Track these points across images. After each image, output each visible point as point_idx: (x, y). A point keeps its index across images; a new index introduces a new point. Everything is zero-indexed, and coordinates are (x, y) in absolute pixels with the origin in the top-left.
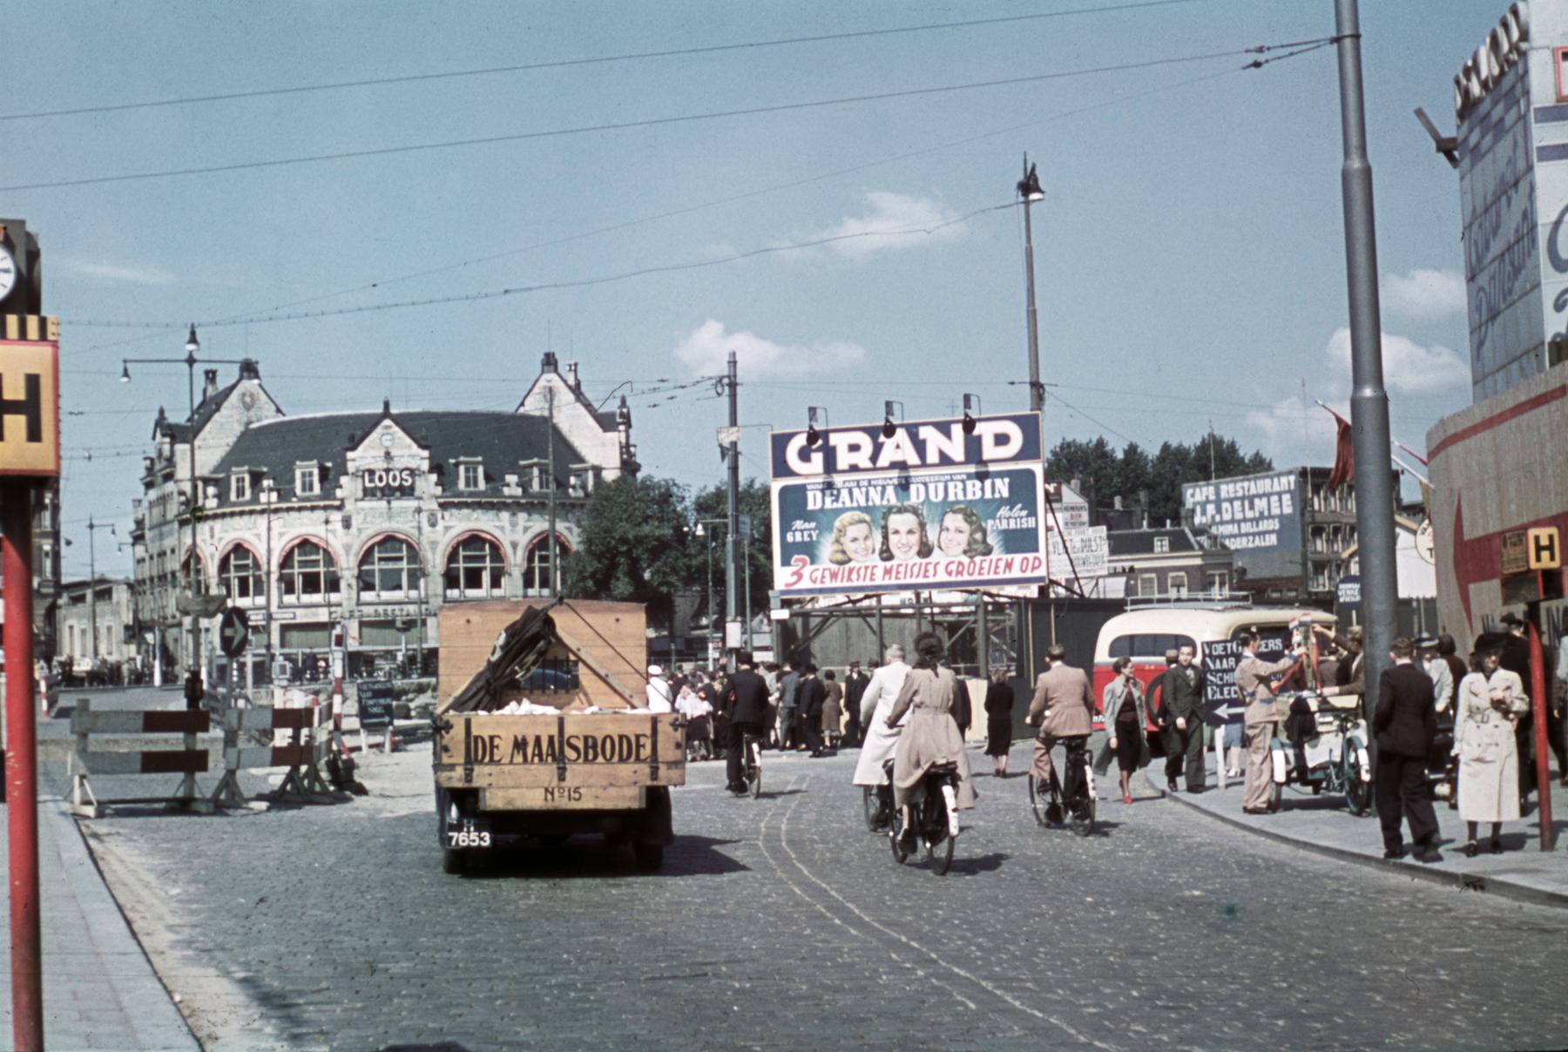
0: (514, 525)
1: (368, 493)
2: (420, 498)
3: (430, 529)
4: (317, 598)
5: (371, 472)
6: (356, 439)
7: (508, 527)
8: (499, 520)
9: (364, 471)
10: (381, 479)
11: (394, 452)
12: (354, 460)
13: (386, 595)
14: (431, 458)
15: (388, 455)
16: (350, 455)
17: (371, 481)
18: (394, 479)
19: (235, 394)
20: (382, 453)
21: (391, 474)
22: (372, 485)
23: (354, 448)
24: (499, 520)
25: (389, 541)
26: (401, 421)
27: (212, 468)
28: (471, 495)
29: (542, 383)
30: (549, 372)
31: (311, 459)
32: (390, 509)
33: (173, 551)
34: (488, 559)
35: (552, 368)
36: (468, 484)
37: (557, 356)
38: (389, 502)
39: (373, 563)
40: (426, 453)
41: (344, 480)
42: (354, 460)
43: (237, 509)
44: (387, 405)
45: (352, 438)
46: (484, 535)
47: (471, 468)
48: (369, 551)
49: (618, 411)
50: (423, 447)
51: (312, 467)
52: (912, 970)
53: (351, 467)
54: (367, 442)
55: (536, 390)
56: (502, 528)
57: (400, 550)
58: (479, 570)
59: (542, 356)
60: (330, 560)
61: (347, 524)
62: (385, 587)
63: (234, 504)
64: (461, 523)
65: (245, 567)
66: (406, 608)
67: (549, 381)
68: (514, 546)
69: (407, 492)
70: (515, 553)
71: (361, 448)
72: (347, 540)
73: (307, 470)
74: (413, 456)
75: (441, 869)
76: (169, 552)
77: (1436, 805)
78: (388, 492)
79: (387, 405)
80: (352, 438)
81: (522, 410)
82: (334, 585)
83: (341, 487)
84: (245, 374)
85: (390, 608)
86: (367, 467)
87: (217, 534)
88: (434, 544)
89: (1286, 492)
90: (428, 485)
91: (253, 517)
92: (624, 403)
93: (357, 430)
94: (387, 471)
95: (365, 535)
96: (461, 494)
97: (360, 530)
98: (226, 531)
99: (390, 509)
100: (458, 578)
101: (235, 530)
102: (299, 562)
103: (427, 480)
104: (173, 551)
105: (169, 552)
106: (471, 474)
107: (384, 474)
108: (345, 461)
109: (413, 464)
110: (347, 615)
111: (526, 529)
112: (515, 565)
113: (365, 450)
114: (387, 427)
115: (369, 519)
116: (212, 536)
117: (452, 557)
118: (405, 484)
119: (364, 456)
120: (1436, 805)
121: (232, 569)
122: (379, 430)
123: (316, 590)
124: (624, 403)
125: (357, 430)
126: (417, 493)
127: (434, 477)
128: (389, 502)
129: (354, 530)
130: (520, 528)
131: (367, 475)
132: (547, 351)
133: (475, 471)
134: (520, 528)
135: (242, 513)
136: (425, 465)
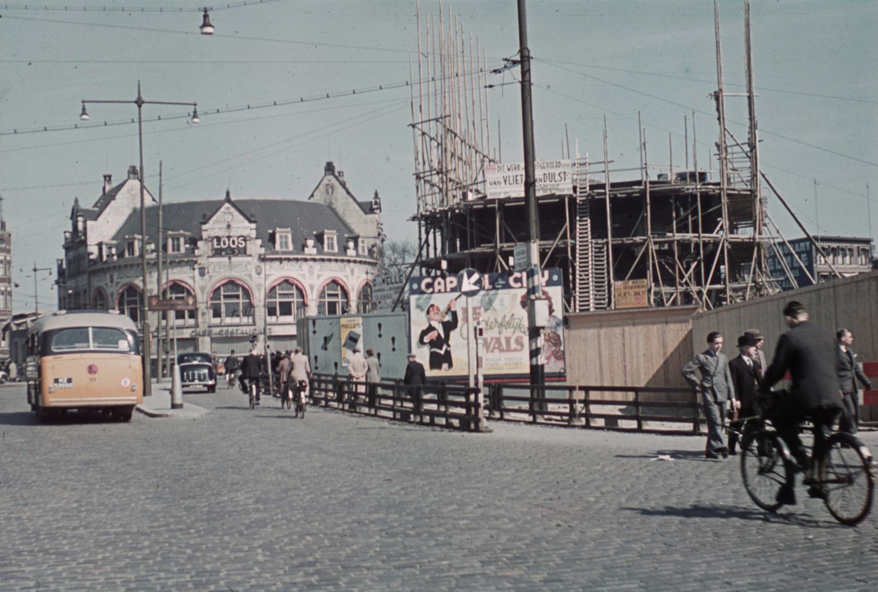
0: (311, 273)
1: (218, 253)
2: (250, 256)
3: (257, 276)
4: (236, 320)
5: (219, 239)
6: (207, 217)
7: (307, 275)
8: (302, 270)
9: (213, 238)
10: (224, 244)
11: (233, 225)
12: (206, 230)
13: (228, 320)
14: (256, 229)
15: (229, 226)
16: (204, 227)
17: (219, 244)
18: (234, 242)
19: (124, 189)
20: (225, 226)
21: (231, 239)
22: (219, 247)
23: (205, 223)
24: (302, 270)
25: (232, 283)
26: (234, 204)
27: (111, 238)
28: (283, 253)
29: (325, 181)
30: (329, 175)
31: (287, 227)
32: (230, 263)
33: (85, 292)
34: (340, 296)
35: (331, 172)
36: (281, 247)
37: (334, 164)
38: (230, 259)
39: (275, 297)
40: (253, 226)
41: (200, 244)
42: (206, 230)
43: (326, 257)
44: (228, 193)
45: (204, 216)
46: (183, 284)
47: (176, 239)
48: (217, 291)
49: (373, 201)
50: (250, 221)
51: (288, 232)
52: (194, 551)
53: (205, 235)
54: (214, 218)
55: (321, 187)
56: (303, 276)
57: (337, 290)
58: (136, 309)
59: (324, 164)
60: (301, 293)
61: (202, 274)
62: (282, 314)
63: (329, 254)
64: (276, 272)
65: (135, 302)
66: (240, 328)
67: (329, 181)
68: (312, 287)
69: (243, 252)
70: (312, 292)
71: (211, 221)
72: (202, 283)
73: (284, 234)
74: (246, 228)
75: (850, 488)
76: (82, 293)
77: (717, 427)
78: (231, 252)
79: (228, 193)
80: (204, 216)
81: (312, 200)
82: (193, 314)
83: (198, 248)
84: (132, 176)
85: (230, 329)
86: (215, 235)
87: (115, 280)
88: (259, 286)
89: (803, 252)
90: (256, 247)
91: (299, 263)
92: (376, 194)
93: (208, 210)
94: (229, 237)
95: (213, 280)
96: (277, 253)
97: (211, 277)
98: (121, 278)
99: (230, 263)
100: (275, 309)
101: (128, 277)
102: (128, 301)
103: (255, 243)
104: (85, 292)
105: (82, 293)
106: (284, 240)
107: (226, 239)
108: (201, 231)
109: (245, 233)
110: (201, 334)
111: (319, 276)
112: (312, 300)
113: (214, 224)
114: (228, 208)
115: (217, 269)
116: (112, 281)
117: (322, 295)
118: (240, 246)
119: (213, 228)
120: (717, 427)
121: (222, 297)
122: (223, 209)
123: (183, 317)
124: (376, 194)
125: (208, 210)
126: (248, 252)
127: (259, 242)
128: (230, 259)
129: (207, 277)
130: (315, 276)
131: (215, 240)
132: (328, 161)
133: (178, 239)
134: (315, 276)
135: (330, 260)
136: (253, 234)
